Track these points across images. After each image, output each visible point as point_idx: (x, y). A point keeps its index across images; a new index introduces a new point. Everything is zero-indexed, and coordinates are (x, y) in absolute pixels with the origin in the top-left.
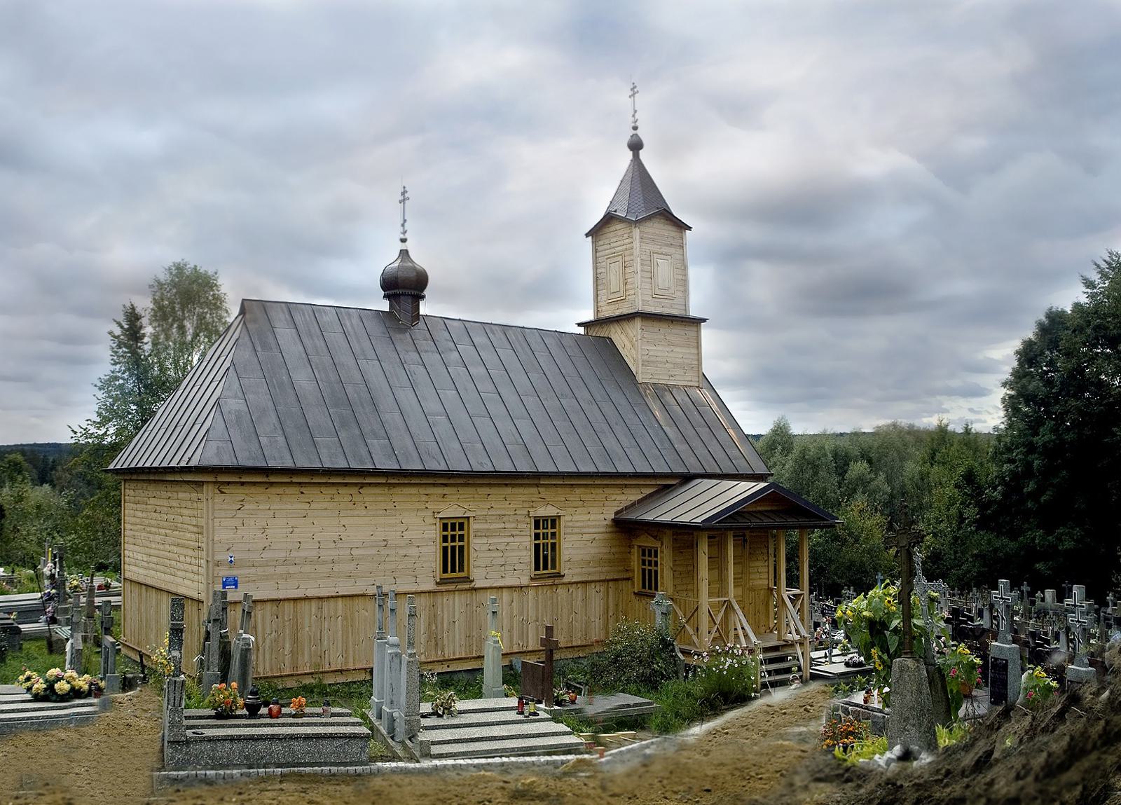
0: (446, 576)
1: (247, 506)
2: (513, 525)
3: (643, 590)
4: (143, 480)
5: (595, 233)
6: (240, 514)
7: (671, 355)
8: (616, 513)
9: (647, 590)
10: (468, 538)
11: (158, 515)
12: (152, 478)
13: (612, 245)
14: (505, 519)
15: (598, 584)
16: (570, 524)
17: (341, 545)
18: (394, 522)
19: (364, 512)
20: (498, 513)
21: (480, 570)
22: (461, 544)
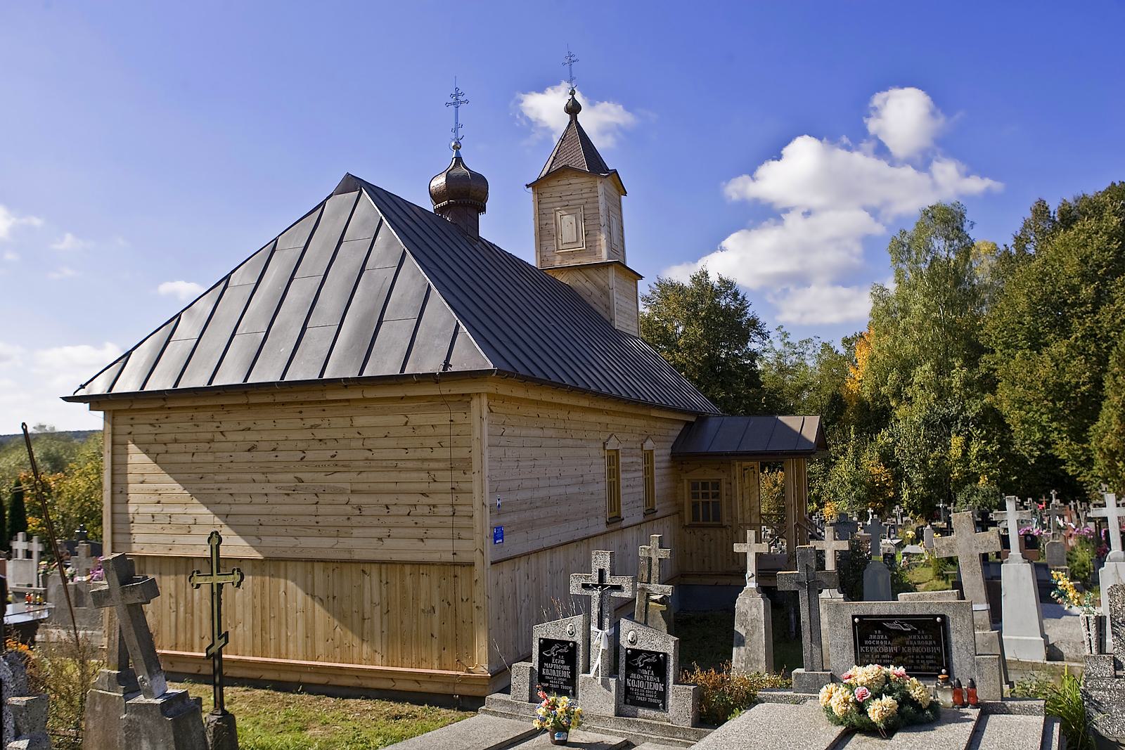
13: (564, 198)
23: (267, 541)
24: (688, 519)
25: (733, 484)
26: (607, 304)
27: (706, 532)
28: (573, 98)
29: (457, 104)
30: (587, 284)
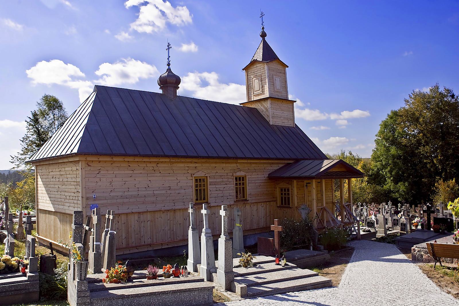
0: (197, 202)
1: (102, 172)
2: (226, 180)
3: (282, 205)
4: (46, 164)
5: (246, 69)
6: (98, 176)
7: (282, 114)
8: (269, 174)
9: (287, 205)
10: (207, 185)
11: (54, 180)
12: (51, 162)
13: (255, 73)
14: (223, 177)
15: (262, 203)
16: (251, 179)
17: (148, 189)
18: (173, 179)
19: (159, 175)
20: (220, 175)
21: (212, 199)
22: (243, 182)
23: (57, 206)
24: (279, 203)
25: (293, 189)
26: (268, 114)
27: (285, 209)
28: (263, 31)
29: (169, 49)
30: (262, 107)
